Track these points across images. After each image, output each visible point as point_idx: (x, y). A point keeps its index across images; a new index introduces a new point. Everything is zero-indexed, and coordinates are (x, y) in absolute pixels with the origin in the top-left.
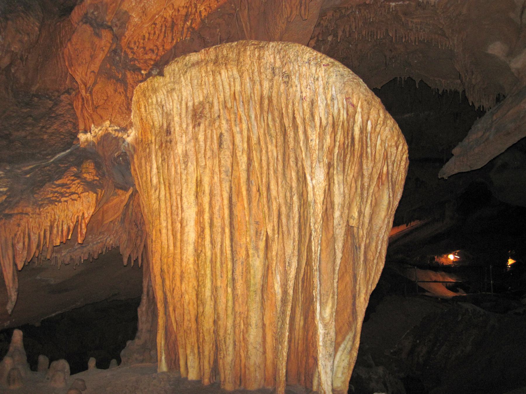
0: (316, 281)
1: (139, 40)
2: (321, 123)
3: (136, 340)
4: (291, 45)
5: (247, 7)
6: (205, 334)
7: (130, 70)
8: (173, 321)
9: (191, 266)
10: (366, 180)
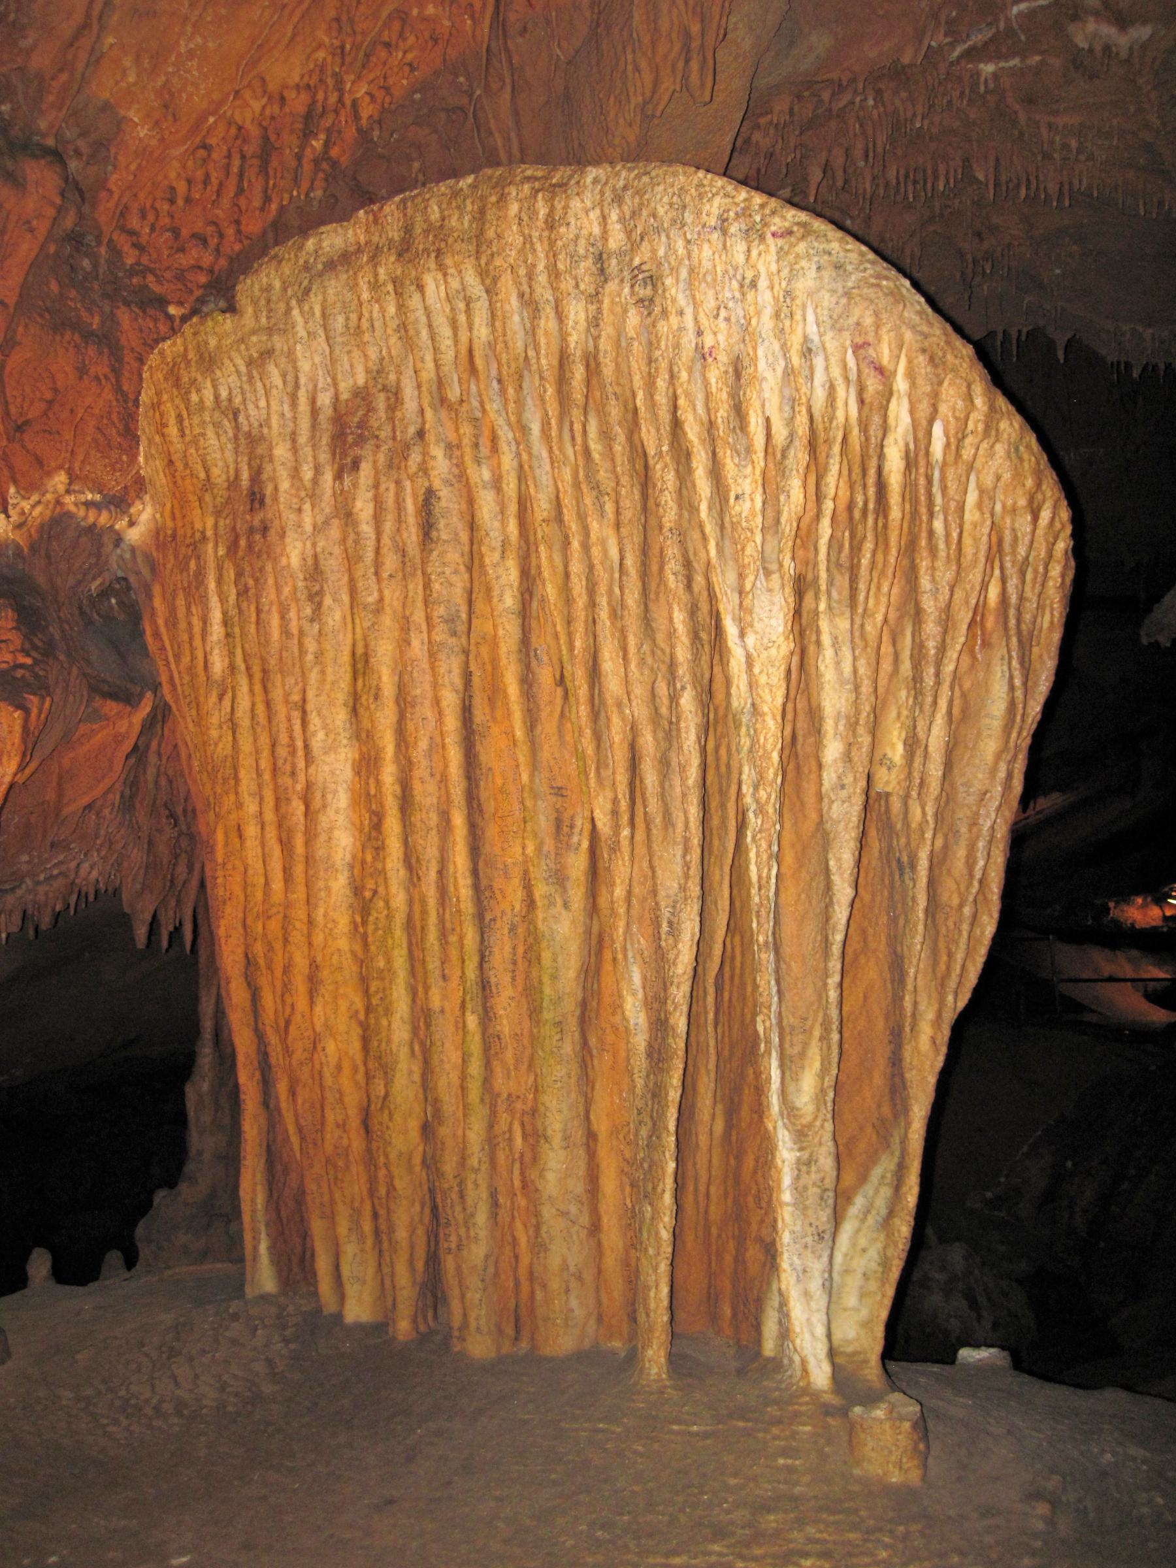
0: (766, 982)
1: (157, 205)
2: (769, 436)
3: (183, 1187)
4: (658, 171)
5: (508, 80)
6: (396, 1171)
7: (127, 304)
8: (291, 1129)
9: (343, 944)
10: (931, 628)
